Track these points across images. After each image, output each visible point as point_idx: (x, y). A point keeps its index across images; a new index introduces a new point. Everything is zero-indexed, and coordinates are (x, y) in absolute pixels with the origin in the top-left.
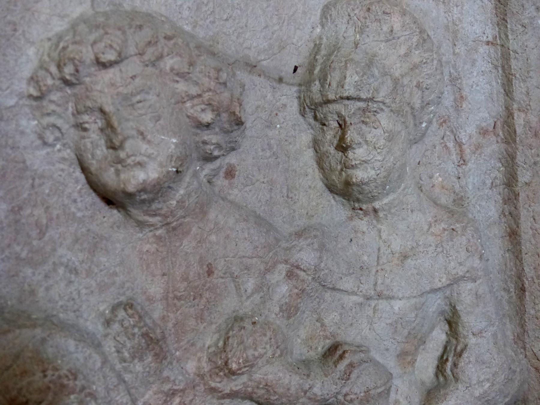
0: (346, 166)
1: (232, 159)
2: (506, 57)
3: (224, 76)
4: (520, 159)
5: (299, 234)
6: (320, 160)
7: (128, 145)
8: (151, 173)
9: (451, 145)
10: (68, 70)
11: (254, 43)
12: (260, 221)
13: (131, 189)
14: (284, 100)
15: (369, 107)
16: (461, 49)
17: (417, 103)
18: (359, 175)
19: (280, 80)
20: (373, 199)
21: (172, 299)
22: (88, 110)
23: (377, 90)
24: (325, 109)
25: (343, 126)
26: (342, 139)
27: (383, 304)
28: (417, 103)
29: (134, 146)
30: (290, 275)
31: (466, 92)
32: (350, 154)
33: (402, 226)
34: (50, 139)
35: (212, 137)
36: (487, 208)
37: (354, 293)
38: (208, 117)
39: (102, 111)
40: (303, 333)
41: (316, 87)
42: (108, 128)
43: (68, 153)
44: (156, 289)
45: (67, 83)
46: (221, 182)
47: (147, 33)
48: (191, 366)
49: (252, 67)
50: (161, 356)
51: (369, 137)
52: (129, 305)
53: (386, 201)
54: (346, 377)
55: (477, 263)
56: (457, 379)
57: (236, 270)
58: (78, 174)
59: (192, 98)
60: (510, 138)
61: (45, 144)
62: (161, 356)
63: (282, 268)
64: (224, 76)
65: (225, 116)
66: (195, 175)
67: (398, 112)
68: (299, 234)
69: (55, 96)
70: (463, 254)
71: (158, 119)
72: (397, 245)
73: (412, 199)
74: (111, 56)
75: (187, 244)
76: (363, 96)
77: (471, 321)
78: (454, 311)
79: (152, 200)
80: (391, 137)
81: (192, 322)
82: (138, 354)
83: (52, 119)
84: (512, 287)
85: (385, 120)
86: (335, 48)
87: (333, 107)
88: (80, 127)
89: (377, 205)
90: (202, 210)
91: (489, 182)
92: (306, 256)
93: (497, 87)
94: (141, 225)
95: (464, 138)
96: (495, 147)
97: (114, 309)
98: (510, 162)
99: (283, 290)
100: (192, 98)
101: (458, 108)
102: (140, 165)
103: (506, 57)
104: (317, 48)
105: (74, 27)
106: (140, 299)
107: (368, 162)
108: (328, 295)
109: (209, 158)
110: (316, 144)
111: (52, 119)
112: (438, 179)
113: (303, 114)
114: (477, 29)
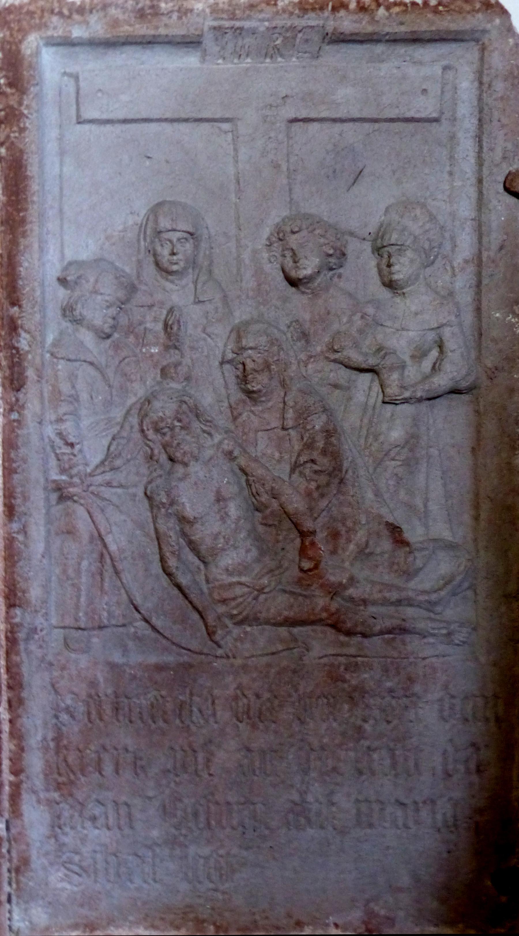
0: (391, 273)
1: (341, 270)
2: (480, 226)
3: (339, 236)
4: (484, 273)
5: (369, 302)
6: (380, 272)
7: (301, 262)
8: (308, 272)
9: (448, 268)
10: (281, 235)
11: (354, 225)
12: (350, 295)
13: (301, 277)
14: (365, 247)
15: (401, 248)
16: (457, 223)
17: (427, 246)
18: (396, 277)
19: (364, 239)
20: (402, 288)
21: (312, 322)
22: (287, 249)
23: (406, 241)
24: (383, 250)
25: (390, 256)
26: (389, 261)
27: (404, 333)
28: (427, 246)
29: (303, 262)
30: (362, 317)
31: (458, 242)
32: (392, 268)
33: (416, 301)
34: (272, 260)
35: (333, 260)
36: (466, 298)
37: (391, 327)
38: (331, 252)
39: (292, 250)
40: (367, 342)
41: (379, 241)
42: (294, 254)
43: (278, 266)
44: (307, 317)
45: (280, 240)
46: (336, 279)
47: (310, 221)
48: (319, 349)
49: (352, 234)
50: (308, 342)
51: (401, 261)
52: (297, 321)
53: (408, 289)
54: (384, 357)
55: (453, 318)
56: (440, 370)
57: (339, 313)
58: (281, 273)
59: (325, 244)
60: (480, 264)
61: (270, 262)
62: (308, 342)
63: (359, 315)
64: (339, 236)
65: (338, 252)
66: (325, 275)
67: (415, 250)
68: (369, 302)
69: (275, 245)
70: (446, 314)
71: (312, 252)
72: (413, 308)
73: (423, 289)
74: (296, 229)
75: (320, 302)
76: (399, 243)
77: (450, 344)
78: (441, 340)
79: (308, 282)
80: (412, 261)
81: (320, 332)
82: (299, 339)
83: (274, 253)
84: (476, 334)
85: (409, 254)
86: (389, 224)
87: (386, 249)
88: (284, 256)
89: (404, 291)
90: (327, 289)
91: (468, 286)
92: (370, 310)
93: (475, 239)
94: (303, 293)
95: (455, 265)
96: (472, 268)
97: (291, 322)
98: (479, 275)
99: (358, 323)
100: (325, 244)
101: (453, 251)
102: (305, 268)
103: (480, 226)
104: (381, 225)
105: (283, 220)
106: (301, 320)
107: (401, 271)
108: (379, 328)
109: (331, 269)
110: (378, 265)
111: (274, 253)
112: (440, 283)
113: (373, 253)
114: (467, 213)
